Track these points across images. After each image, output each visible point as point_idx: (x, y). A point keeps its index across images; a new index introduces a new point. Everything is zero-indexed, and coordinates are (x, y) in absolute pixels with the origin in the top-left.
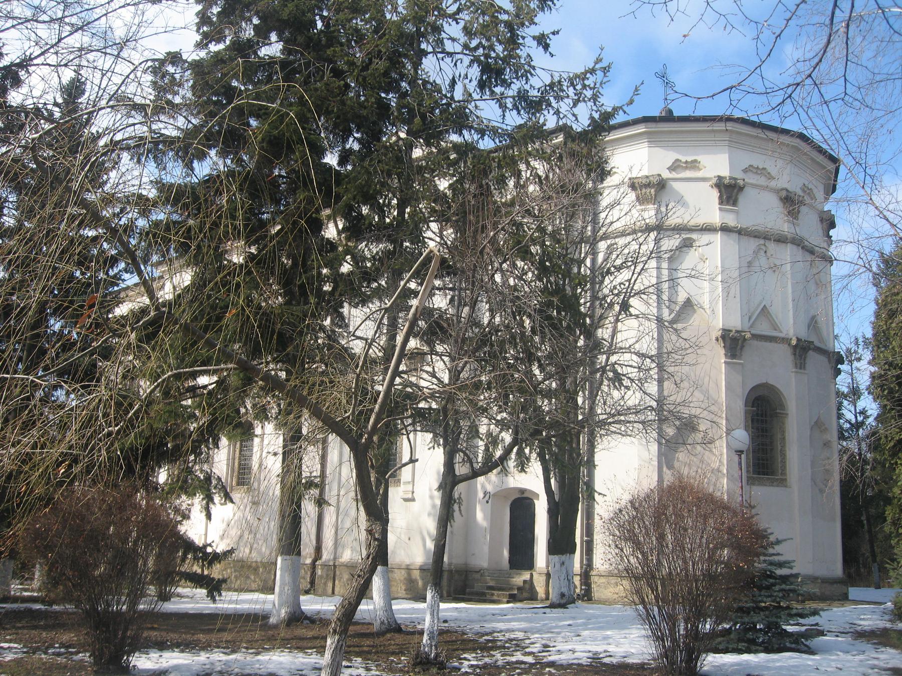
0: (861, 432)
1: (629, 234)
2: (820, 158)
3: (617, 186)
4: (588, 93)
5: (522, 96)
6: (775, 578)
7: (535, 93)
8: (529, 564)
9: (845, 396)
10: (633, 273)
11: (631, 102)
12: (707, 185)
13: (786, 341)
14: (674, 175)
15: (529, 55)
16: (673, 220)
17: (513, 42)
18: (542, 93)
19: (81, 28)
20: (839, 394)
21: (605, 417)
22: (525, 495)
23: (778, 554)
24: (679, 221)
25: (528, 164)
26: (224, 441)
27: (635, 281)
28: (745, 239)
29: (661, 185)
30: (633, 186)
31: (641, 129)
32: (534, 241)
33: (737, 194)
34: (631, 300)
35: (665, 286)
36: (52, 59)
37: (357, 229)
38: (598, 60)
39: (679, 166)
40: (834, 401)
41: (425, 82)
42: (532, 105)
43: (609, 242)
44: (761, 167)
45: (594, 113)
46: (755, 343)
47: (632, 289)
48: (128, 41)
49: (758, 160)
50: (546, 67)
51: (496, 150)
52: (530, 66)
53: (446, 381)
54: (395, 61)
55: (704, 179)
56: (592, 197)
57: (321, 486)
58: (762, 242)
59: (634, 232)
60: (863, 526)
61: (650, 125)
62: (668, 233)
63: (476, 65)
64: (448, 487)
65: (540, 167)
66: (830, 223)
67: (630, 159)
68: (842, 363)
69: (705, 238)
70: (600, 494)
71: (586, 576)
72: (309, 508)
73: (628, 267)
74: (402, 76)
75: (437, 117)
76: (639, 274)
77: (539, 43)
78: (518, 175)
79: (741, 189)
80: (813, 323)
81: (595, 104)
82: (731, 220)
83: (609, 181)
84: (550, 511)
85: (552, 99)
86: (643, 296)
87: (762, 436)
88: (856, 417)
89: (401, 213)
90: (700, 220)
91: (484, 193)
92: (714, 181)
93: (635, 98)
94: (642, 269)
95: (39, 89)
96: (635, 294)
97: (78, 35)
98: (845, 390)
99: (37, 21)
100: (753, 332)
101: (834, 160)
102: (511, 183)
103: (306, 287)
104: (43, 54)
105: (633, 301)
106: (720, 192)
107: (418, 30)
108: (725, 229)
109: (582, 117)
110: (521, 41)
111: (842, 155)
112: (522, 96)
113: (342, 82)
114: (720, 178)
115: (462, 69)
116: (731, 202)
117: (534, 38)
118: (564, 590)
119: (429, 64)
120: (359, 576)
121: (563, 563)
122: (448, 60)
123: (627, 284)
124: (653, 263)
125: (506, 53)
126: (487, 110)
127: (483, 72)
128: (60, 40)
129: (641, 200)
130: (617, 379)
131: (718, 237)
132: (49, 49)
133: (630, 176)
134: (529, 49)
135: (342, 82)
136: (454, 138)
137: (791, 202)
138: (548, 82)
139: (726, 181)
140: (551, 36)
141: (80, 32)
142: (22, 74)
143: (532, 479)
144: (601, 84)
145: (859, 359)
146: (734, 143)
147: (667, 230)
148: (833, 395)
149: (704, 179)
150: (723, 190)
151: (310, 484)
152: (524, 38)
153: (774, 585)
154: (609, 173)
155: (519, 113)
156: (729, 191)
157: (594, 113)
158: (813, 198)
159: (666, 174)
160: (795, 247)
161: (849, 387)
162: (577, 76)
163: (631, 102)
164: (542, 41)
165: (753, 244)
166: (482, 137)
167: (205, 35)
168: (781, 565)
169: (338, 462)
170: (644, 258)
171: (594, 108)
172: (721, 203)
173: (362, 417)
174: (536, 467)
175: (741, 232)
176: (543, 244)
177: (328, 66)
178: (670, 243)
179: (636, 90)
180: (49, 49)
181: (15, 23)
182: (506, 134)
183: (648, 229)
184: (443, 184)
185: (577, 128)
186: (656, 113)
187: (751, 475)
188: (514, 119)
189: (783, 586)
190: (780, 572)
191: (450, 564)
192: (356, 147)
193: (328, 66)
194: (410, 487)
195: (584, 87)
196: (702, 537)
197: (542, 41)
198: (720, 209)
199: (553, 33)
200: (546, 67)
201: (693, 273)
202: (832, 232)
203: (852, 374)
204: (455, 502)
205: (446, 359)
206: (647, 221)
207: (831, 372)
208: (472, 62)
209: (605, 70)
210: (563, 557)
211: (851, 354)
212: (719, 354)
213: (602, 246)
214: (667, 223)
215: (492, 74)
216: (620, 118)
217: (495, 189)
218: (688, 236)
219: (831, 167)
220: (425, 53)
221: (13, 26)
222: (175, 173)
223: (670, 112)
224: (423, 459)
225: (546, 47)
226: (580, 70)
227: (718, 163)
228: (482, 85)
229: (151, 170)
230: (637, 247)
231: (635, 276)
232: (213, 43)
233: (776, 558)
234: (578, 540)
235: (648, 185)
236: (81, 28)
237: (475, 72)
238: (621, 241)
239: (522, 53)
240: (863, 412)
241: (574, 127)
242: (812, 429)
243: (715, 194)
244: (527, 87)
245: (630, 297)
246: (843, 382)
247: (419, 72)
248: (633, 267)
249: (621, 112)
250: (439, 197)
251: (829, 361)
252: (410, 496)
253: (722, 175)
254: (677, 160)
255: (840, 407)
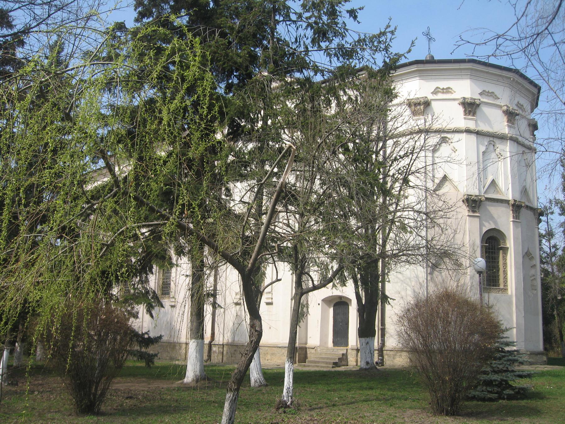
0: (553, 259)
1: (408, 135)
2: (504, 73)
3: (400, 104)
4: (383, 46)
5: (341, 47)
6: (504, 352)
7: (348, 46)
8: (345, 343)
9: (544, 236)
10: (411, 160)
11: (409, 51)
12: (456, 103)
13: (507, 202)
14: (435, 97)
15: (344, 22)
16: (436, 126)
17: (333, 14)
18: (353, 46)
19: (62, 8)
20: (541, 236)
21: (397, 251)
22: (343, 300)
23: (506, 337)
24: (440, 126)
25: (345, 93)
26: (155, 268)
27: (413, 164)
28: (481, 138)
29: (427, 104)
30: (409, 105)
31: (414, 68)
32: (349, 140)
33: (476, 109)
34: (410, 176)
35: (429, 168)
36: (43, 27)
37: (236, 133)
38: (388, 26)
39: (439, 92)
40: (537, 239)
41: (279, 40)
42: (347, 53)
43: (395, 140)
44: (490, 91)
45: (386, 58)
46: (488, 203)
47: (410, 170)
48: (91, 16)
49: (490, 88)
50: (354, 31)
51: (323, 82)
52: (345, 29)
53: (297, 229)
54: (260, 26)
55: (454, 100)
56: (383, 111)
57: (214, 296)
58: (491, 139)
59: (411, 133)
60: (554, 318)
61: (420, 65)
62: (432, 135)
63: (309, 28)
64: (298, 297)
65: (352, 93)
66: (534, 127)
67: (409, 88)
68: (543, 216)
69: (457, 136)
70: (391, 299)
71: (381, 351)
72: (208, 309)
73: (408, 156)
74: (264, 38)
75: (286, 61)
76: (415, 160)
77: (351, 16)
78: (338, 98)
79: (478, 105)
80: (525, 192)
81: (387, 53)
82: (471, 125)
83: (395, 101)
84: (359, 310)
85: (358, 50)
86: (417, 174)
87: (492, 262)
88: (550, 249)
89: (265, 123)
90: (452, 126)
91: (316, 111)
92: (461, 100)
93: (412, 48)
94: (417, 157)
95: (35, 47)
96: (413, 173)
97: (59, 13)
98: (543, 232)
99: (33, 4)
100: (486, 196)
101: (536, 86)
102: (333, 105)
103: (205, 172)
104: (38, 25)
105: (411, 178)
106: (465, 107)
107: (274, 7)
108: (468, 131)
109: (378, 61)
110: (338, 14)
111: (539, 82)
112: (341, 47)
113: (227, 41)
114: (464, 98)
115: (301, 31)
116: (472, 114)
117: (348, 11)
118: (369, 360)
119: (282, 30)
120: (246, 354)
121: (368, 343)
122: (293, 26)
123: (407, 166)
124: (422, 154)
125: (329, 21)
126: (318, 57)
127: (315, 34)
128: (49, 16)
129: (414, 113)
130: (403, 228)
131: (464, 135)
132: (42, 21)
133: (408, 98)
134: (344, 18)
135: (227, 41)
136: (297, 75)
137: (511, 115)
138: (356, 39)
139: (469, 101)
140: (358, 11)
141: (61, 10)
142: (23, 37)
143: (349, 291)
144: (390, 40)
145: (552, 213)
146: (474, 75)
147: (431, 132)
148: (537, 236)
149: (454, 100)
150: (467, 106)
151: (208, 295)
152: (340, 12)
153: (504, 356)
154: (396, 96)
155: (338, 59)
156: (471, 107)
157: (386, 58)
158: (524, 110)
159: (430, 97)
160: (512, 142)
161: (545, 230)
162: (374, 36)
163: (409, 51)
164: (353, 13)
165: (486, 141)
166: (316, 75)
167: (140, 13)
168: (507, 344)
169: (230, 280)
170: (418, 150)
171: (386, 55)
172: (465, 114)
173: (246, 253)
174: (350, 283)
175: (478, 133)
176: (354, 143)
177: (218, 31)
178: (433, 140)
179: (413, 43)
180: (42, 21)
181: (20, 5)
182: (330, 71)
183: (420, 131)
184: (290, 105)
185: (376, 68)
186: (423, 58)
187: (485, 286)
188: (336, 63)
189: (510, 357)
190: (507, 349)
191: (330, 307)
192: (236, 81)
193: (218, 31)
194: (270, 296)
195: (380, 42)
196: (461, 328)
197: (353, 13)
198: (465, 118)
199: (360, 9)
200: (354, 31)
201: (449, 159)
202: (536, 133)
203: (547, 222)
204: (304, 306)
205: (297, 216)
206: (420, 126)
207: (535, 221)
208: (307, 26)
209: (392, 33)
210: (368, 339)
211: (547, 210)
212: (464, 210)
213: (390, 143)
214: (432, 128)
215: (321, 34)
216: (403, 61)
217: (324, 107)
218: (444, 135)
219: (535, 91)
220: (278, 22)
221: (19, 8)
222: (122, 99)
223: (433, 57)
224: (279, 279)
225: (355, 17)
226: (377, 32)
227: (465, 88)
228: (313, 41)
229: (106, 98)
230: (414, 143)
231: (412, 161)
232: (146, 18)
233: (505, 340)
234: (376, 329)
235: (419, 104)
236: (62, 8)
237: (310, 33)
238: (402, 140)
239: (340, 20)
240: (555, 246)
241: (374, 67)
242: (523, 257)
243: (461, 109)
244: (343, 42)
245: (409, 175)
246: (543, 227)
247: (275, 34)
248: (411, 156)
249: (403, 57)
250: (288, 112)
251: (534, 214)
252: (270, 301)
253: (466, 97)
254: (437, 88)
255: (540, 241)
